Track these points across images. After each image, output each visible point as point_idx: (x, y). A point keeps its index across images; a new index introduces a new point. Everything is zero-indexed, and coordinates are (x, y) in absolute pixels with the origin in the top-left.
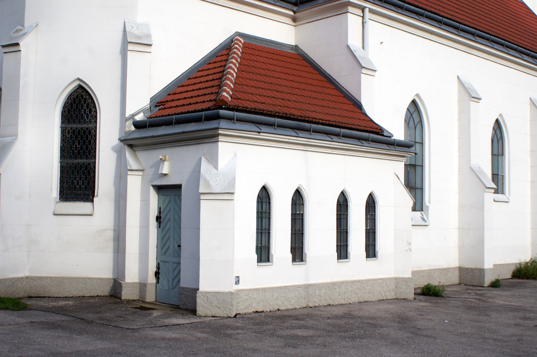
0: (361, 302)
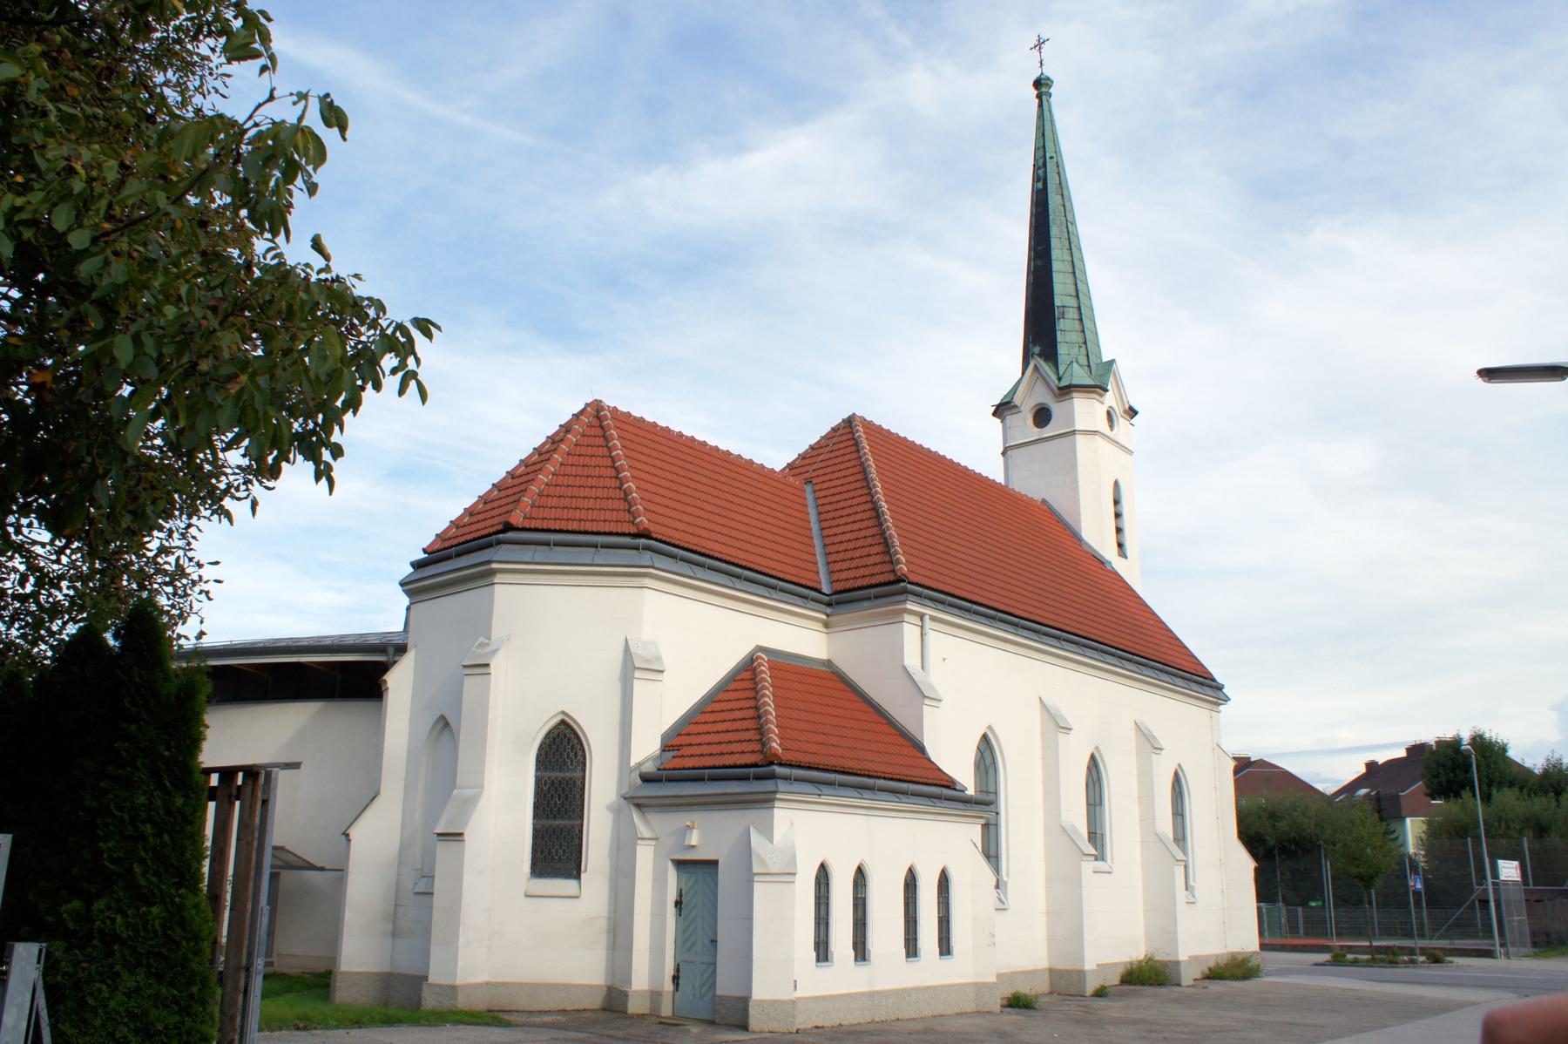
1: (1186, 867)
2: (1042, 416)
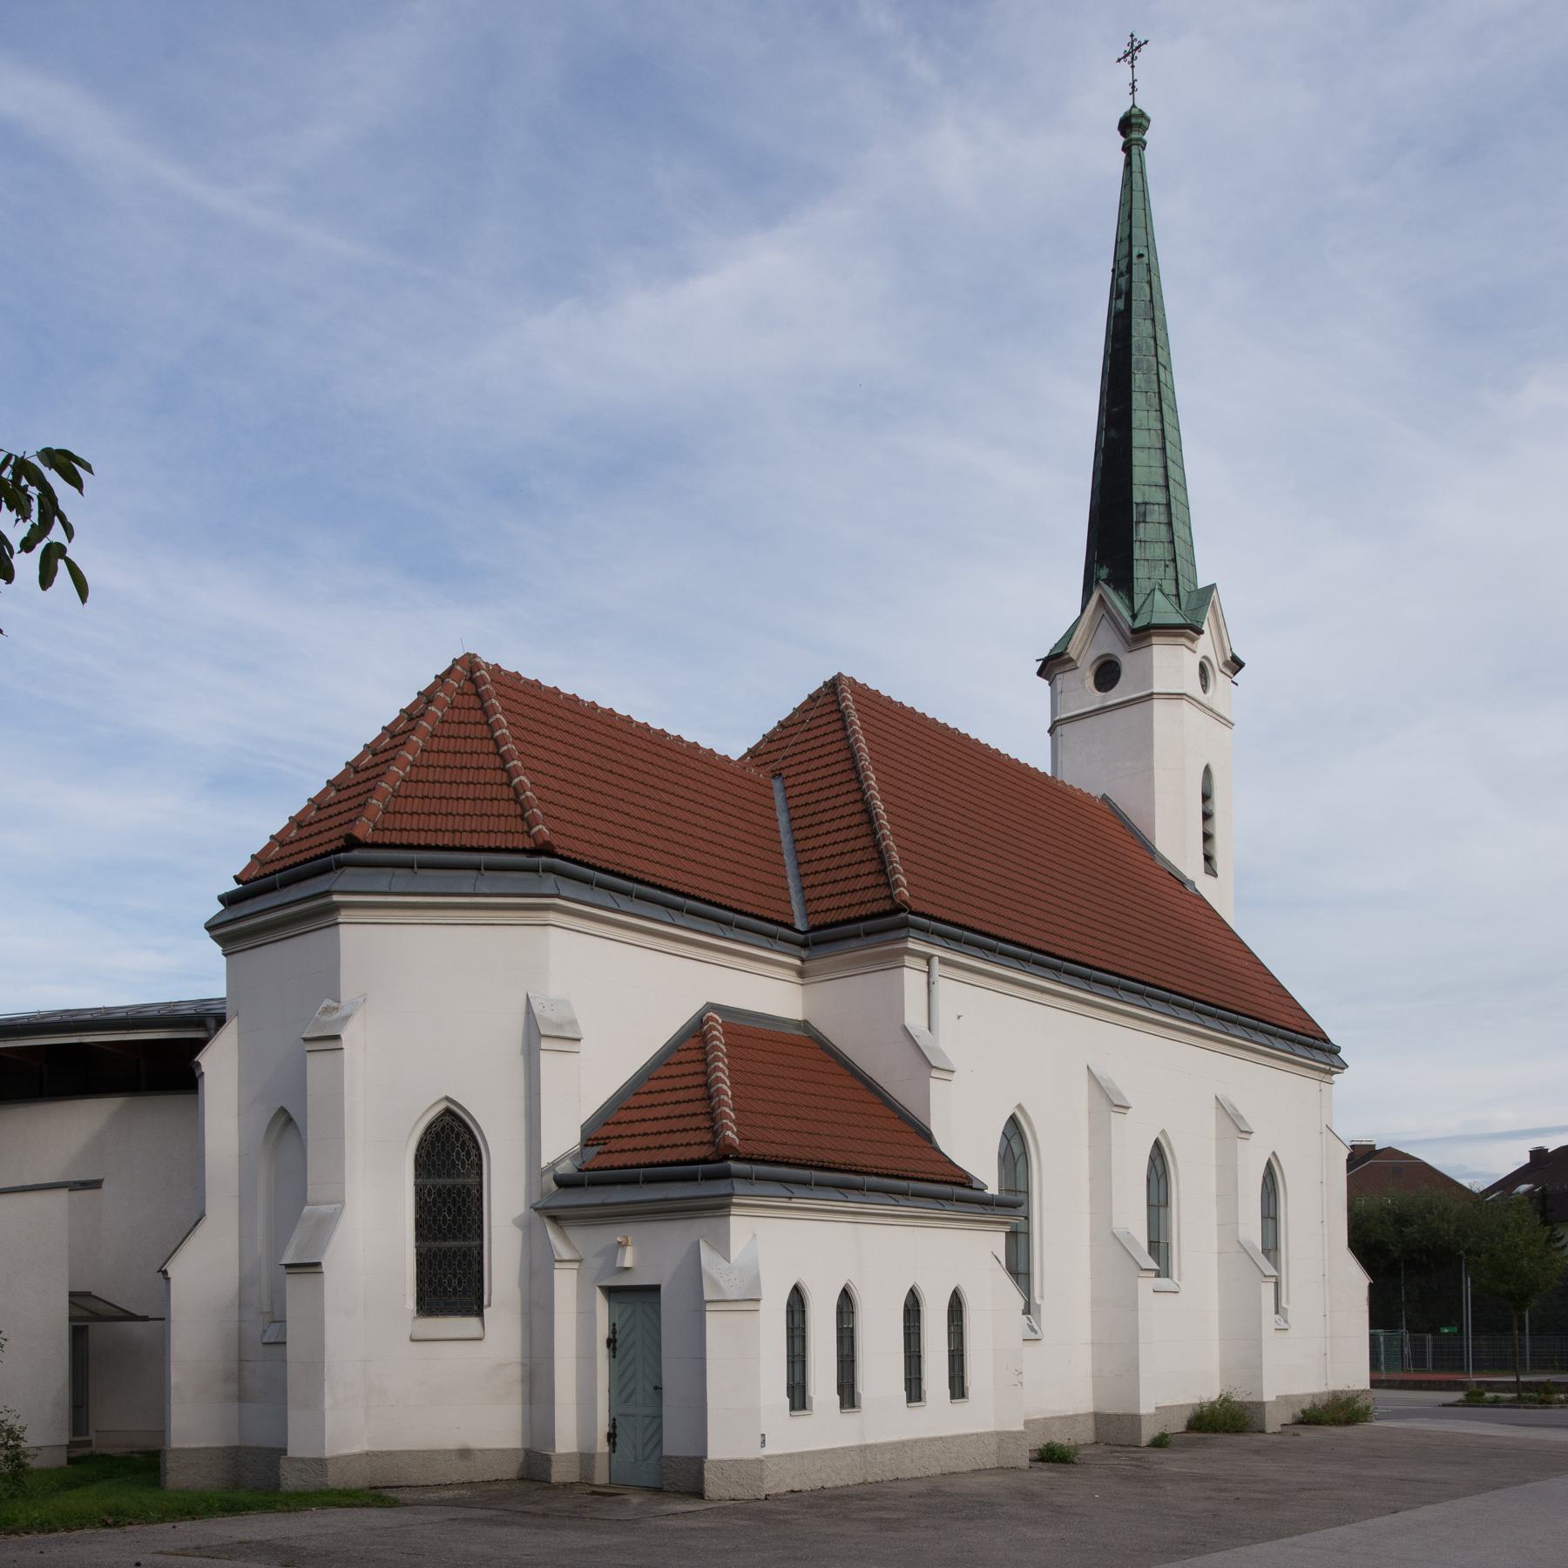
0: (944, 1474)
1: (1277, 1285)
2: (1107, 674)
